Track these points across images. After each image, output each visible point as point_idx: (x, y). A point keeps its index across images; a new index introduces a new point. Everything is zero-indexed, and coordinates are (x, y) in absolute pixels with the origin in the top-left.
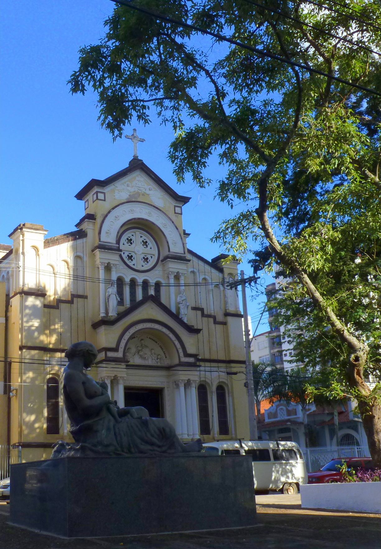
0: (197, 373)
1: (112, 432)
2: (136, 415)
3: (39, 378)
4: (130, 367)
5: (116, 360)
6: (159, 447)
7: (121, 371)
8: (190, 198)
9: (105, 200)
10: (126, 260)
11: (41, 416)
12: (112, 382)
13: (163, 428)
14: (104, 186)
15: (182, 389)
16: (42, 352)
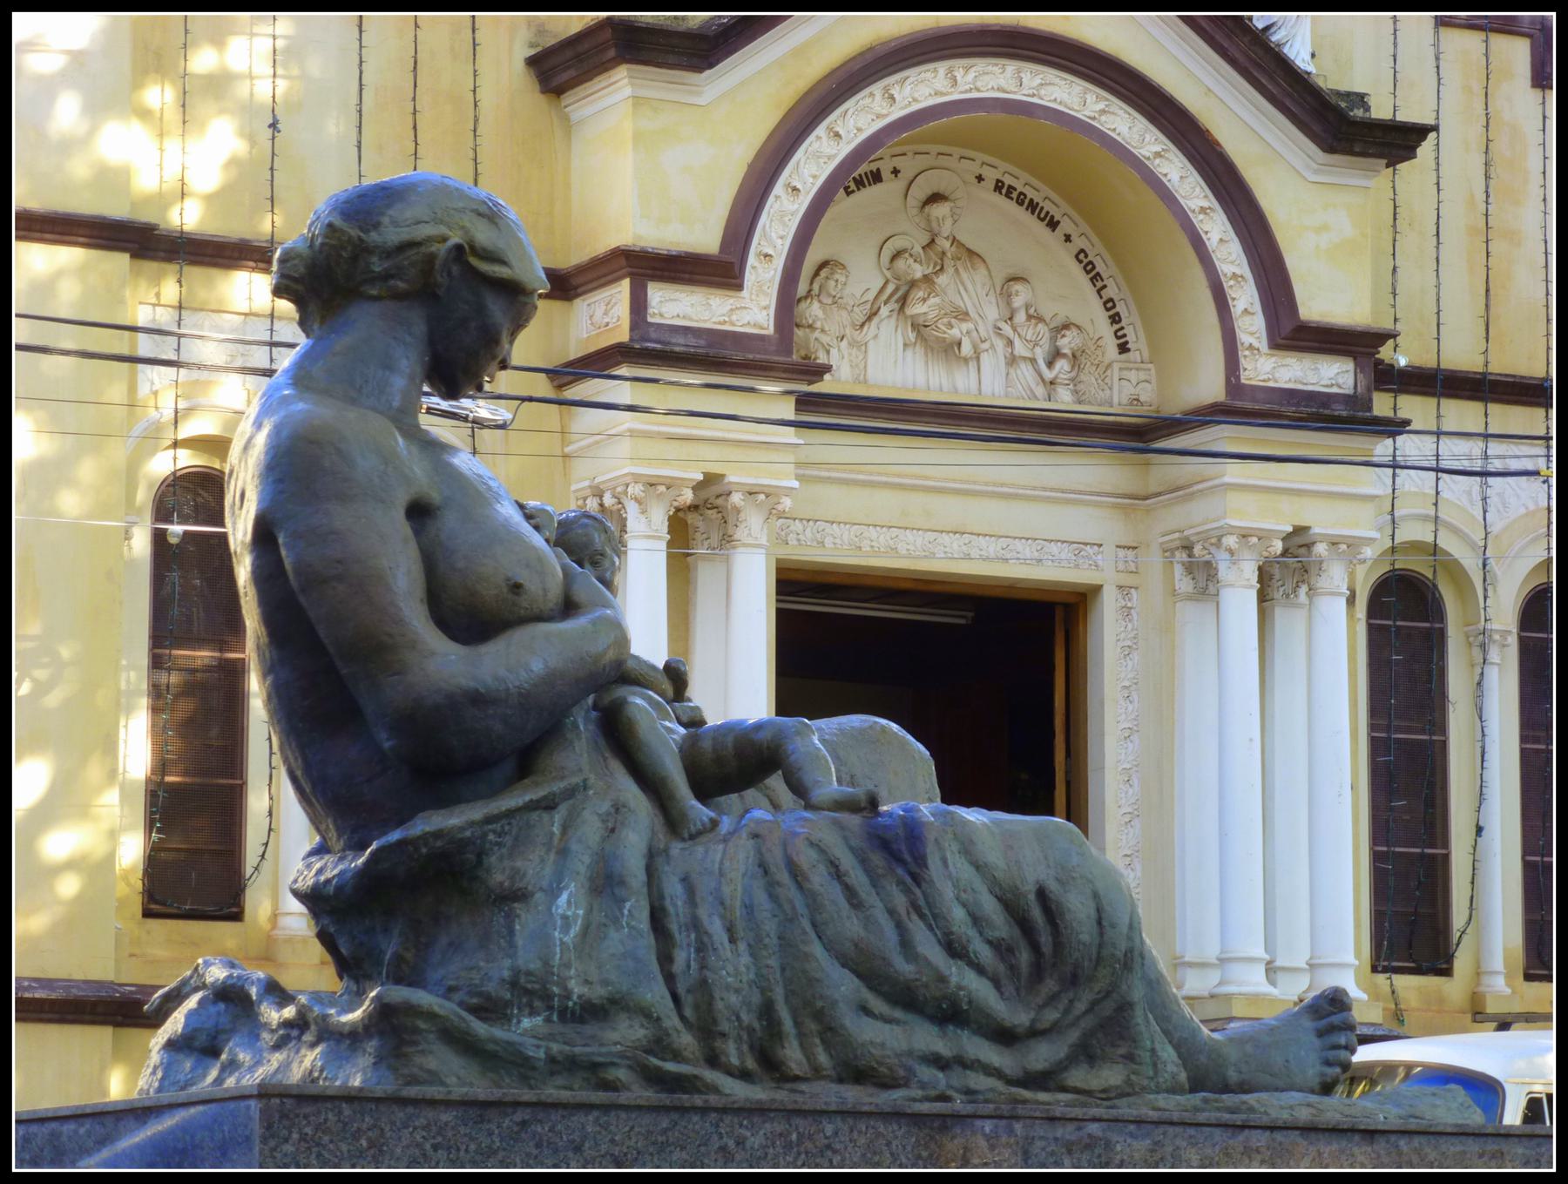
0: (1374, 482)
1: (637, 910)
2: (829, 785)
3: (87, 470)
4: (825, 410)
5: (716, 356)
6: (1005, 1036)
7: (749, 440)
11: (94, 771)
12: (681, 530)
13: (1042, 894)
15: (1240, 600)
16: (119, 261)
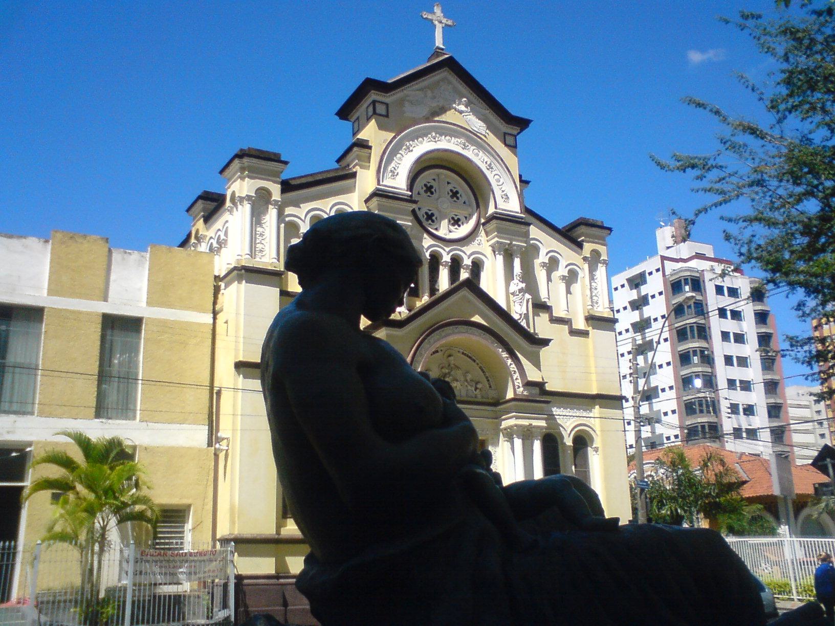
8: (550, 340)
9: (387, 116)
10: (423, 220)
14: (387, 92)
